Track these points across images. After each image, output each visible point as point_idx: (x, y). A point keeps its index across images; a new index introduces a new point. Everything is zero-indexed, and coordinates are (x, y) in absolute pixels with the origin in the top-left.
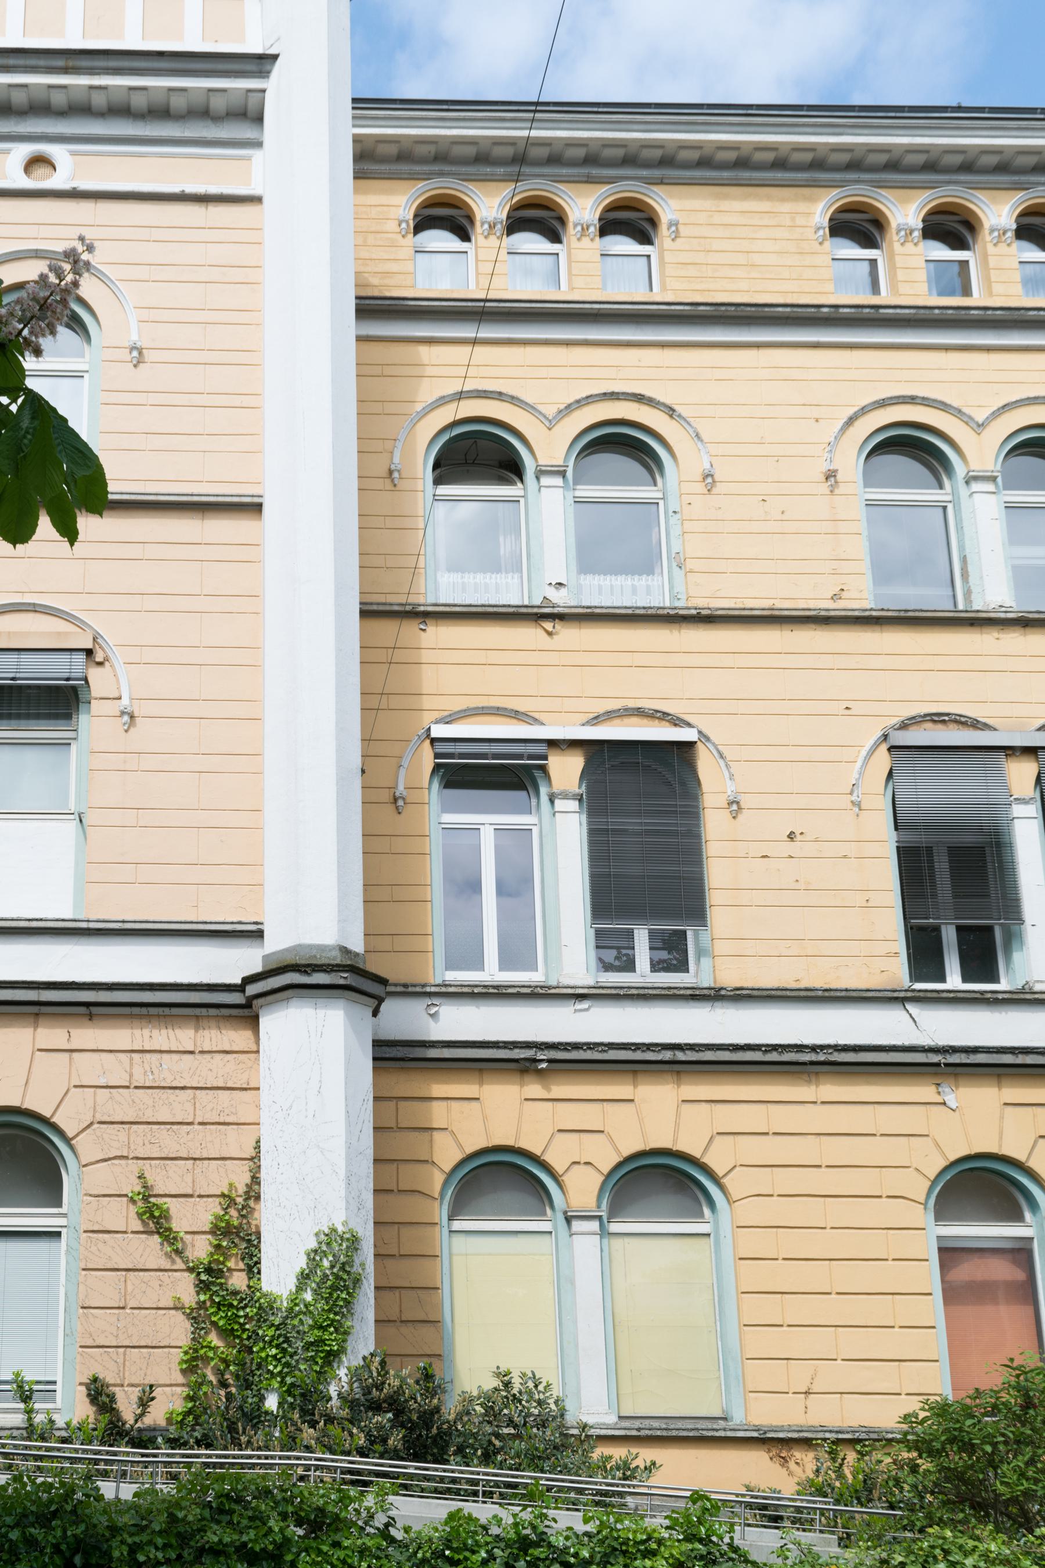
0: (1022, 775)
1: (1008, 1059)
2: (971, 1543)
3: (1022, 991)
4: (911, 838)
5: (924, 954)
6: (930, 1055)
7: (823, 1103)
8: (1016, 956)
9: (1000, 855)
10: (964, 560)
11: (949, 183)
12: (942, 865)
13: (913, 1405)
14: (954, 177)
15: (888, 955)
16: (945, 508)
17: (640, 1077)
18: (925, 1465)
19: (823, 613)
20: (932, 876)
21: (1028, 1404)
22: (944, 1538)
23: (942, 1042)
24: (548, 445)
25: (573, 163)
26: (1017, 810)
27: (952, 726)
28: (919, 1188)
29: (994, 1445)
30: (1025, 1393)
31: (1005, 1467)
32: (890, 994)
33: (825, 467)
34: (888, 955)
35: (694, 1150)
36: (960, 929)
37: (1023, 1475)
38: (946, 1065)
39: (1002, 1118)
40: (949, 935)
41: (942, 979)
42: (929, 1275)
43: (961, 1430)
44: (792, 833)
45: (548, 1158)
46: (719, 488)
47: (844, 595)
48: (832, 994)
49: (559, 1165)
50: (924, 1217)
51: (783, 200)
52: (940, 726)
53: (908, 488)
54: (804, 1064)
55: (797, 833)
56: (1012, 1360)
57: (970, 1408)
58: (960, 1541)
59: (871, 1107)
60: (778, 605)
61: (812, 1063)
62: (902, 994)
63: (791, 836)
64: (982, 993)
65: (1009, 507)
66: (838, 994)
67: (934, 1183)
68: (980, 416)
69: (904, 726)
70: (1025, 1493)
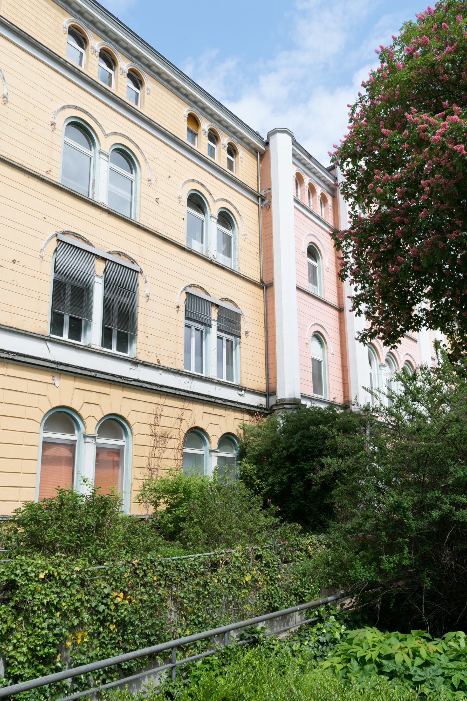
0: (100, 266)
1: (79, 371)
2: (32, 561)
3: (87, 347)
4: (60, 278)
5: (57, 324)
6: (52, 364)
7: (8, 376)
8: (88, 333)
9: (88, 294)
10: (94, 180)
11: (110, 43)
12: (68, 291)
13: (20, 505)
14: (112, 42)
15: (43, 321)
16: (91, 158)
17: (76, 379)
18: (21, 530)
19: (41, 176)
20: (64, 294)
21: (62, 504)
22: (22, 560)
23: (58, 360)
24: (106, 144)
25: (172, 86)
26: (97, 279)
27: (80, 240)
28: (39, 416)
29: (47, 521)
30: (61, 499)
31: (49, 529)
32: (41, 337)
33: (52, 120)
34: (43, 321)
35: (76, 408)
36: (71, 318)
37: (55, 532)
38: (58, 369)
39: (73, 393)
40: (67, 319)
41: (110, 348)
42: (37, 453)
43: (36, 515)
44: (14, 260)
45: (81, 412)
46: (8, 105)
47: (51, 173)
48: (19, 331)
49: (84, 416)
50: (39, 428)
51: (53, 7)
52: (76, 238)
53: (77, 142)
54: (3, 358)
55: (17, 261)
56: (59, 487)
57: (41, 506)
58: (28, 561)
59: (27, 381)
60: (25, 165)
61: (6, 358)
62: (46, 338)
63: (14, 261)
64: (74, 344)
65: (111, 169)
66: (22, 332)
67: (46, 415)
68: (108, 132)
69: (64, 233)
70: (55, 539)
